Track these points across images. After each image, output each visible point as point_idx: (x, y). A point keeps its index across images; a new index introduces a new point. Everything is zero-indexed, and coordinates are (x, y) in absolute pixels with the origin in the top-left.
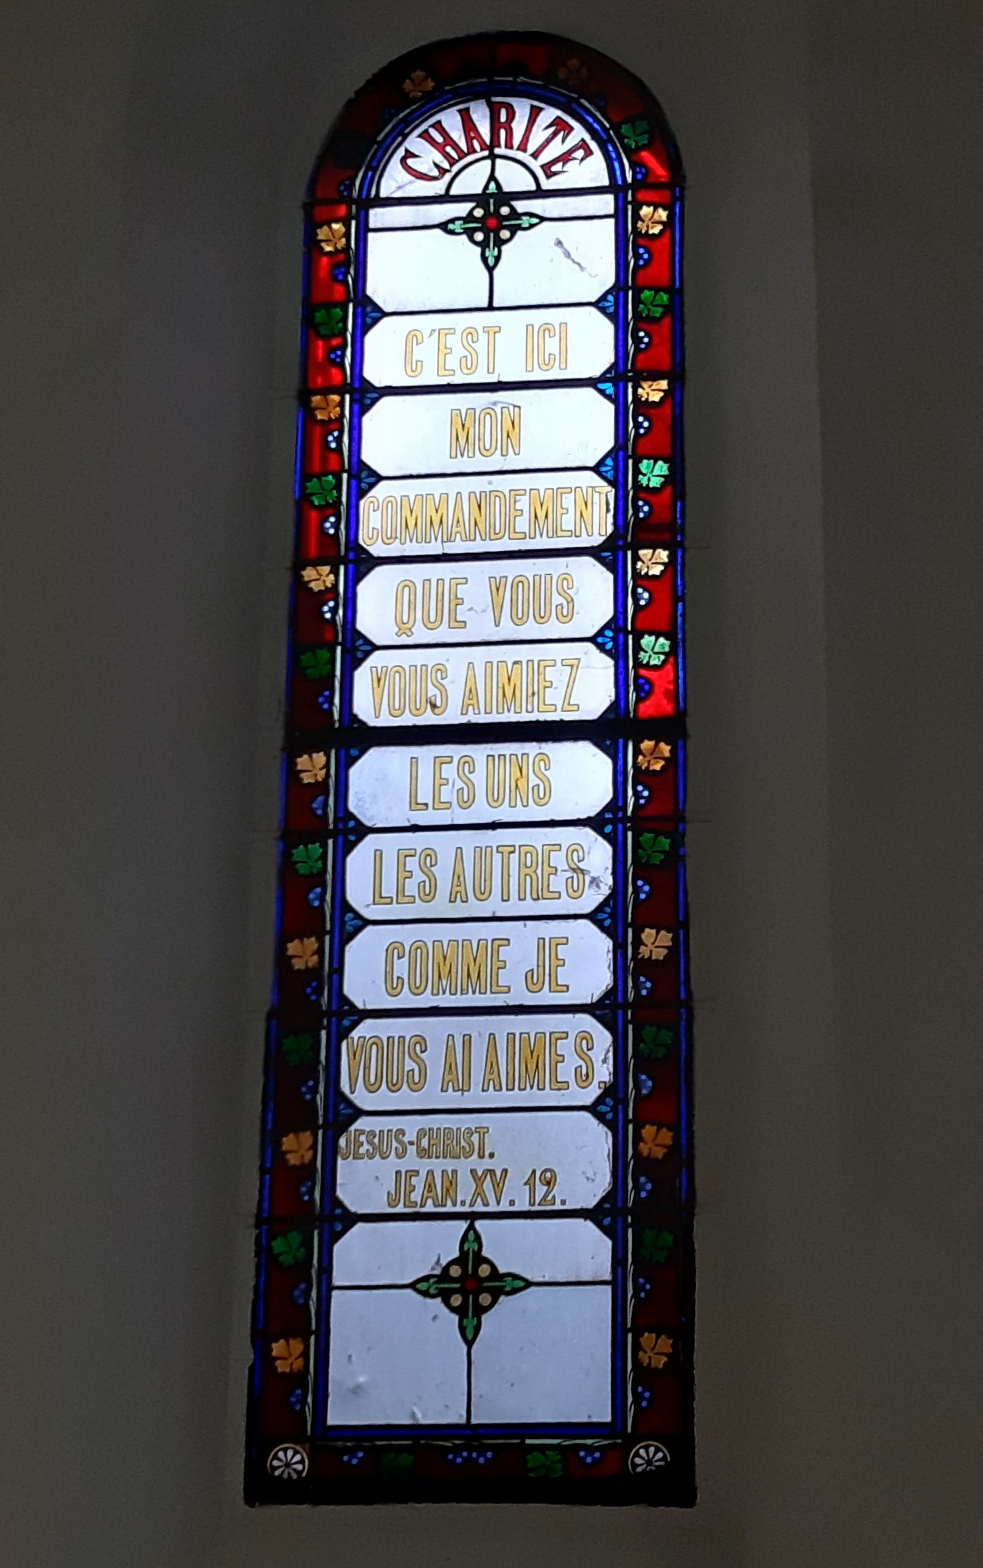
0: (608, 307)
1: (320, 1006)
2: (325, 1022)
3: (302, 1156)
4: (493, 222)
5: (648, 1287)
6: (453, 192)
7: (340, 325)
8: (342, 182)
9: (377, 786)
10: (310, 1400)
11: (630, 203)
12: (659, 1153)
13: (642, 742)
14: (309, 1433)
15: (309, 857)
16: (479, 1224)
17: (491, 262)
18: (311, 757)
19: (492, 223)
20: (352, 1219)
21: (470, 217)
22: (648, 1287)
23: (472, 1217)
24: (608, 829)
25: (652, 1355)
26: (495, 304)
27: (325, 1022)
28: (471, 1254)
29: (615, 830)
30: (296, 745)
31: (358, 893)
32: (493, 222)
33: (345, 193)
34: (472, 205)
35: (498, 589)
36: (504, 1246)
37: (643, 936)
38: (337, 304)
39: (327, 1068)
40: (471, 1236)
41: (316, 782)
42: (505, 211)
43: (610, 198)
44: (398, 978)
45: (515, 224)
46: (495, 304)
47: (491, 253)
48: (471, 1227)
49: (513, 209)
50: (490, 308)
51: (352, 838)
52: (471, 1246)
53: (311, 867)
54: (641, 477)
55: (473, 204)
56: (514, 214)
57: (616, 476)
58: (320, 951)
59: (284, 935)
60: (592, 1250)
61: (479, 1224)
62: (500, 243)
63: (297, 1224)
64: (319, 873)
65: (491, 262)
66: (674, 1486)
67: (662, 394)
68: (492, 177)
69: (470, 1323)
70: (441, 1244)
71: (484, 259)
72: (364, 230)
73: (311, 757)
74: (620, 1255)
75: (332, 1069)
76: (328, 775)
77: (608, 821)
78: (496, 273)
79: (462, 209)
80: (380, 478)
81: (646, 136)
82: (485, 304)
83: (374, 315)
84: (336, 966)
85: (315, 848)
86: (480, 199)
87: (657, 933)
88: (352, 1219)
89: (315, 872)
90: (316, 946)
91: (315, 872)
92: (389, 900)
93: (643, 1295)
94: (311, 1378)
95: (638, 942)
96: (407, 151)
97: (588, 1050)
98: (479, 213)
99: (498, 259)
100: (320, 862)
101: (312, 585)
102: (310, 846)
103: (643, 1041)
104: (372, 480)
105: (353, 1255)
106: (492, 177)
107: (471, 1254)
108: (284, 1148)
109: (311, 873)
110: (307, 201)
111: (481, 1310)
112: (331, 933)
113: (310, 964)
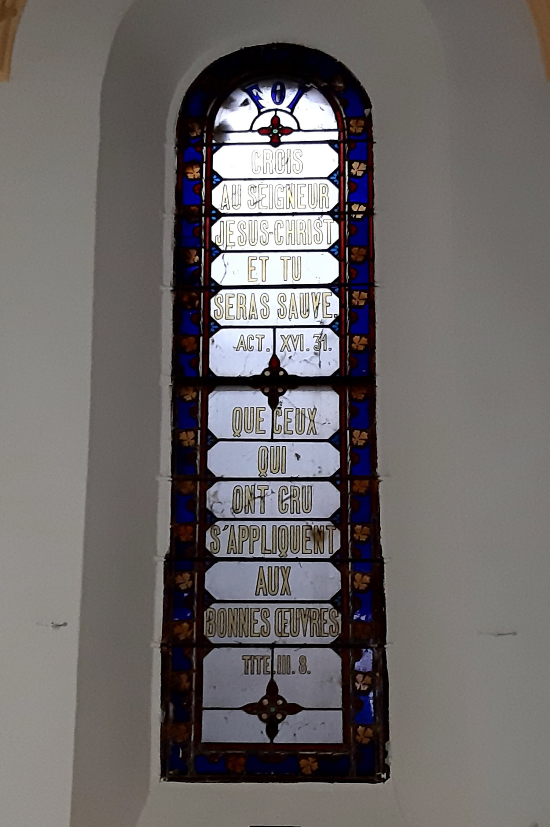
1: (193, 639)
3: (187, 585)
4: (275, 133)
11: (345, 119)
12: (361, 348)
13: (354, 336)
14: (201, 375)
18: (187, 433)
24: (337, 290)
25: (358, 439)
29: (340, 290)
35: (286, 589)
37: (353, 295)
39: (200, 499)
43: (337, 133)
51: (214, 218)
53: (194, 175)
54: (353, 300)
57: (339, 253)
63: (193, 290)
67: (363, 172)
73: (187, 433)
74: (343, 302)
75: (207, 268)
76: (196, 441)
77: (336, 213)
81: (366, 537)
83: (212, 440)
87: (361, 338)
92: (233, 317)
94: (202, 265)
95: (351, 341)
97: (332, 626)
109: (194, 178)
110: (165, 642)
113: (191, 444)
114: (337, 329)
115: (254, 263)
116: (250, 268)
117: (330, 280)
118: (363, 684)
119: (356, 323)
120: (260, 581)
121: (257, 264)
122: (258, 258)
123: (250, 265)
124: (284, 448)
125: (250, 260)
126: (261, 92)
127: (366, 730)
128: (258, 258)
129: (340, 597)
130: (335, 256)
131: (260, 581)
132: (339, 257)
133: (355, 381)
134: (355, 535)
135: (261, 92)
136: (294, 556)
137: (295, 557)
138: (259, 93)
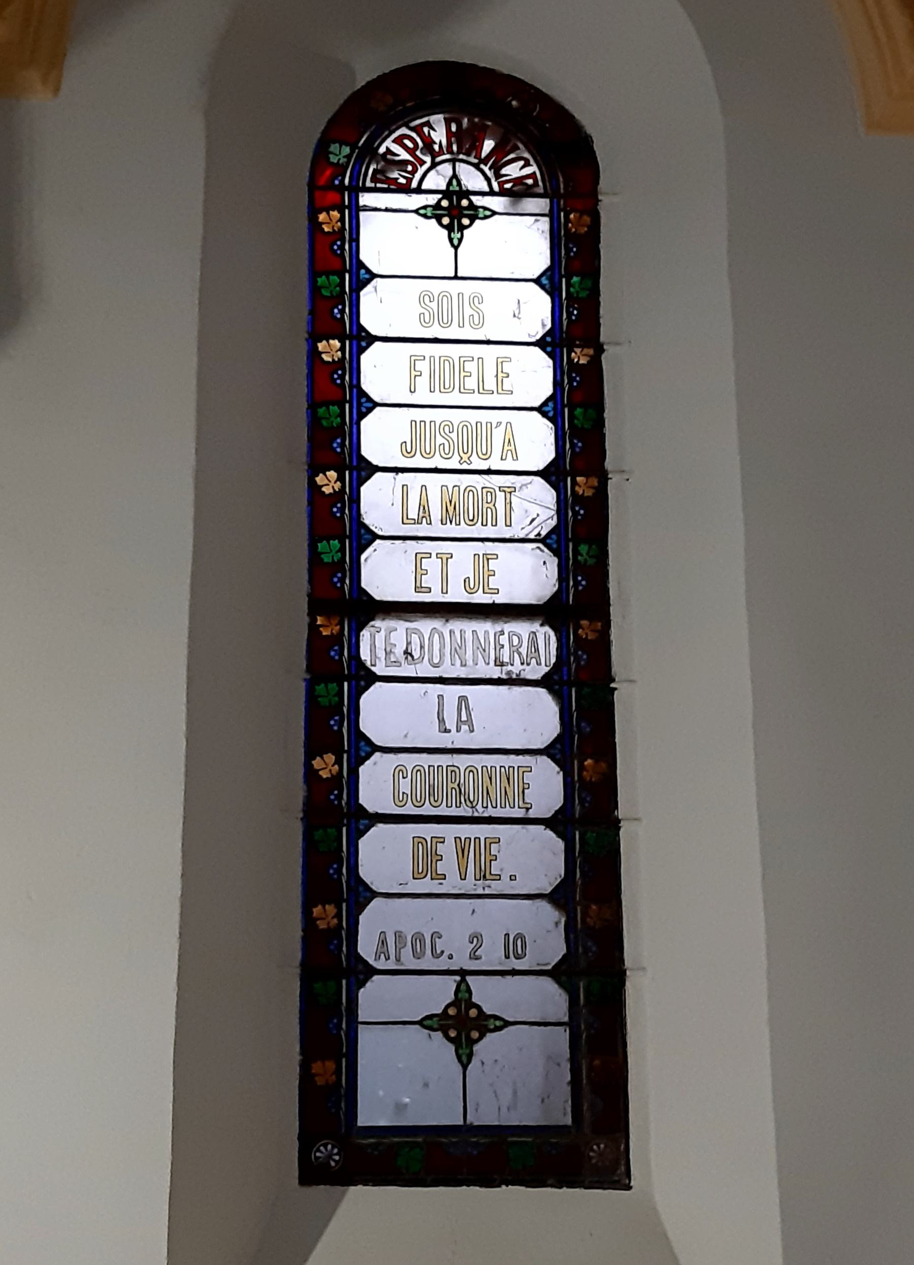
0: (549, 411)
2: (345, 821)
4: (455, 212)
5: (578, 379)
6: (424, 187)
7: (335, 844)
8: (333, 188)
9: (379, 643)
10: (344, 871)
15: (328, 693)
16: (469, 979)
17: (456, 242)
19: (455, 212)
20: (372, 339)
21: (438, 206)
22: (578, 379)
23: (463, 973)
26: (459, 275)
27: (345, 821)
28: (463, 998)
30: (315, 468)
31: (366, 948)
32: (455, 212)
33: (339, 585)
34: (440, 196)
36: (488, 995)
38: (335, 278)
40: (463, 987)
41: (329, 928)
42: (465, 203)
44: (403, 793)
45: (474, 214)
46: (459, 275)
47: (456, 236)
48: (463, 980)
49: (471, 202)
50: (456, 277)
52: (463, 995)
55: (440, 196)
56: (472, 206)
58: (342, 349)
59: (314, 337)
60: (551, 999)
61: (469, 979)
62: (462, 228)
63: (330, 976)
64: (337, 773)
65: (456, 242)
66: (613, 1173)
68: (455, 176)
69: (464, 1051)
70: (438, 995)
71: (451, 240)
72: (356, 209)
77: (549, 344)
78: (459, 250)
79: (432, 199)
80: (376, 405)
82: (453, 275)
84: (354, 236)
85: (333, 687)
86: (446, 194)
88: (372, 339)
89: (336, 359)
90: (335, 911)
91: (336, 359)
93: (575, 384)
96: (387, 148)
98: (445, 203)
99: (460, 240)
100: (339, 554)
101: (324, 489)
102: (331, 542)
103: (573, 286)
104: (370, 405)
105: (373, 999)
106: (455, 176)
107: (463, 998)
108: (313, 1071)
111: (472, 1042)
112: (350, 537)
114: (551, 414)
115: (420, 365)
116: (413, 373)
117: (541, 466)
118: (592, 631)
119: (580, 536)
120: (422, 508)
121: (432, 580)
122: (434, 555)
123: (413, 366)
124: (477, 840)
125: (419, 558)
126: (434, 130)
127: (581, 217)
128: (434, 555)
129: (551, 404)
130: (550, 419)
131: (422, 508)
132: (553, 291)
133: (579, 609)
134: (580, 631)
135: (434, 130)
136: (484, 466)
137: (486, 468)
138: (432, 132)
